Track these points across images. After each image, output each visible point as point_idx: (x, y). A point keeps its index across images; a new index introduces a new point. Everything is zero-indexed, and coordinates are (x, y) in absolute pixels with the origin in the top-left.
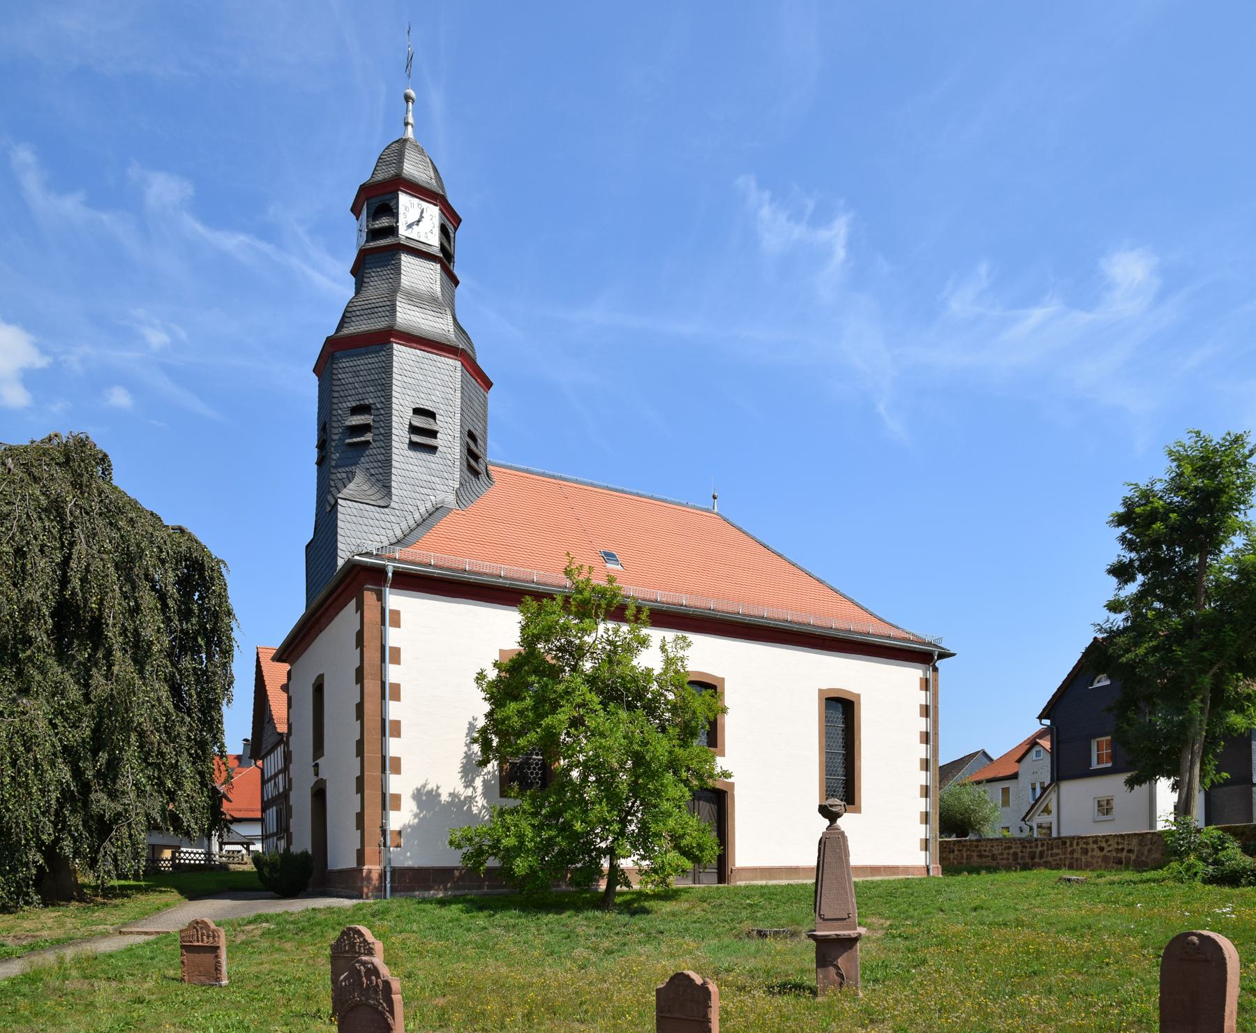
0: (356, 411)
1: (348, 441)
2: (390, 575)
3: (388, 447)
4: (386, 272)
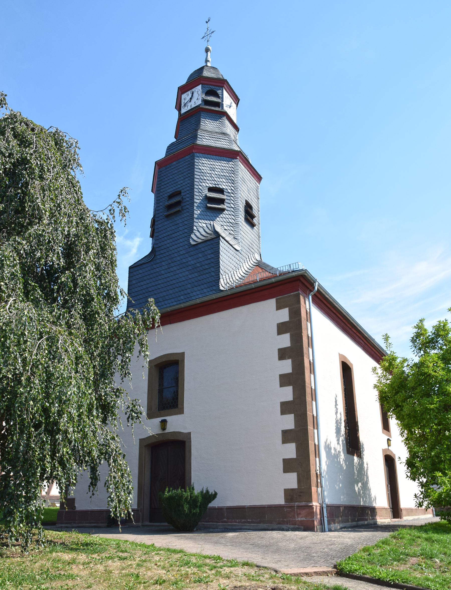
1: (209, 205)
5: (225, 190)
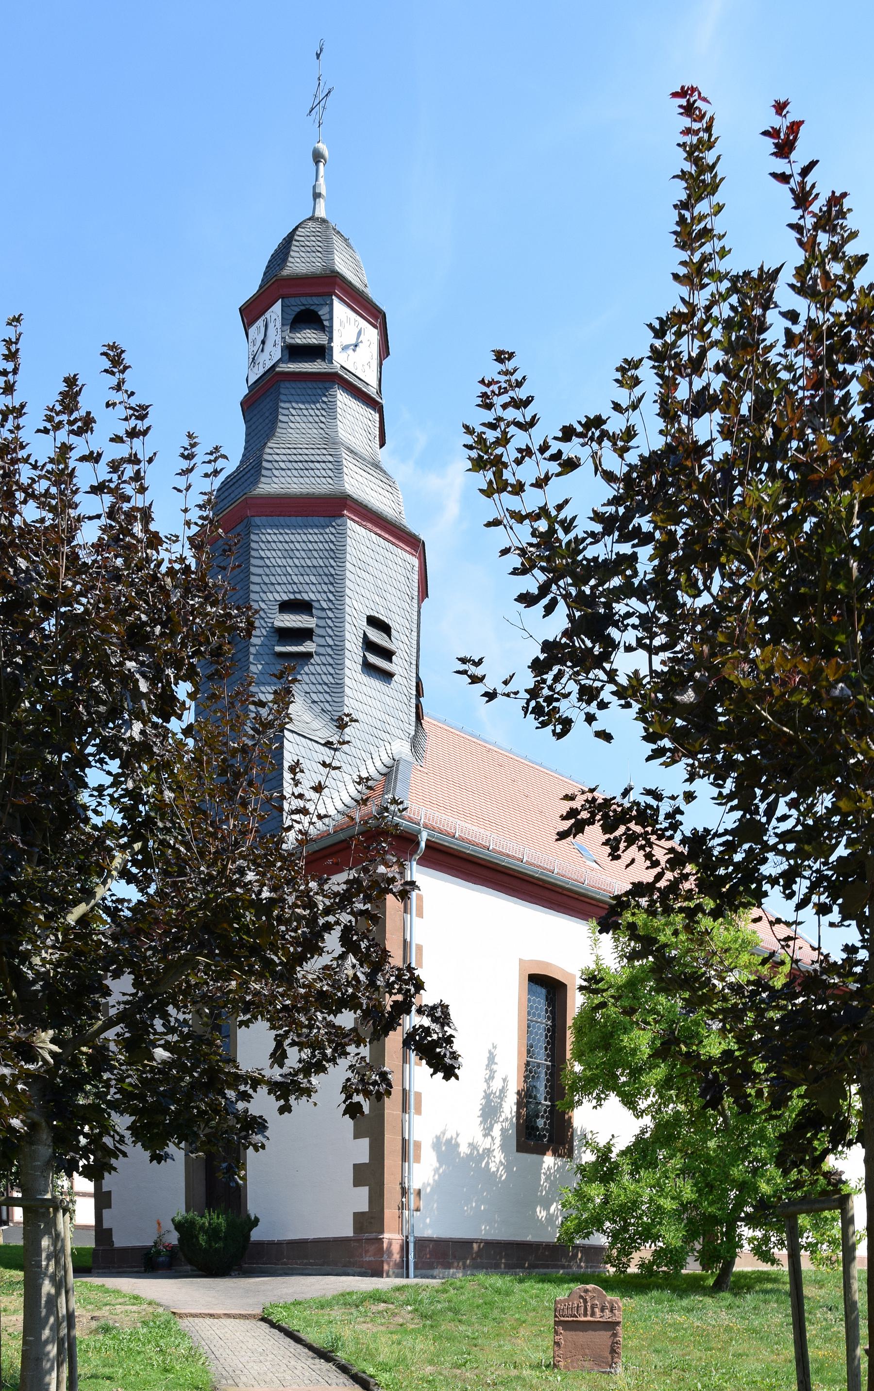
0: (286, 607)
1: (278, 649)
2: (423, 844)
3: (338, 665)
4: (313, 411)
5: (315, 604)
